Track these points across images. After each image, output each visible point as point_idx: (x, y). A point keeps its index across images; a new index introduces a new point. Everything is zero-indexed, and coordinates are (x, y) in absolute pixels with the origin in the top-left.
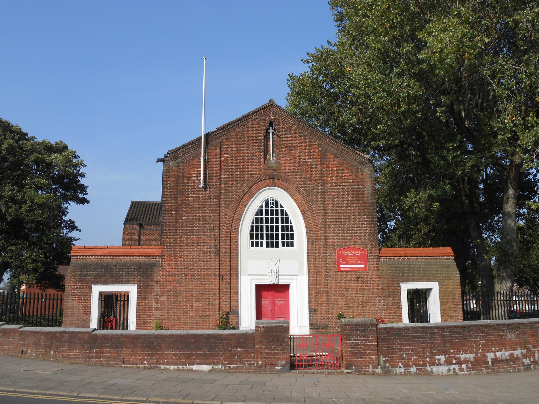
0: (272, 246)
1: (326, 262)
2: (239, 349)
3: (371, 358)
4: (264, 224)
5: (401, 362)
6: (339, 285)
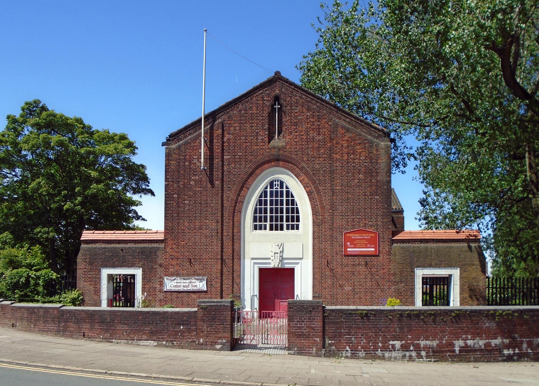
0: (276, 229)
1: (332, 244)
2: (182, 327)
3: (315, 340)
4: (285, 207)
5: (349, 346)
6: (345, 269)
